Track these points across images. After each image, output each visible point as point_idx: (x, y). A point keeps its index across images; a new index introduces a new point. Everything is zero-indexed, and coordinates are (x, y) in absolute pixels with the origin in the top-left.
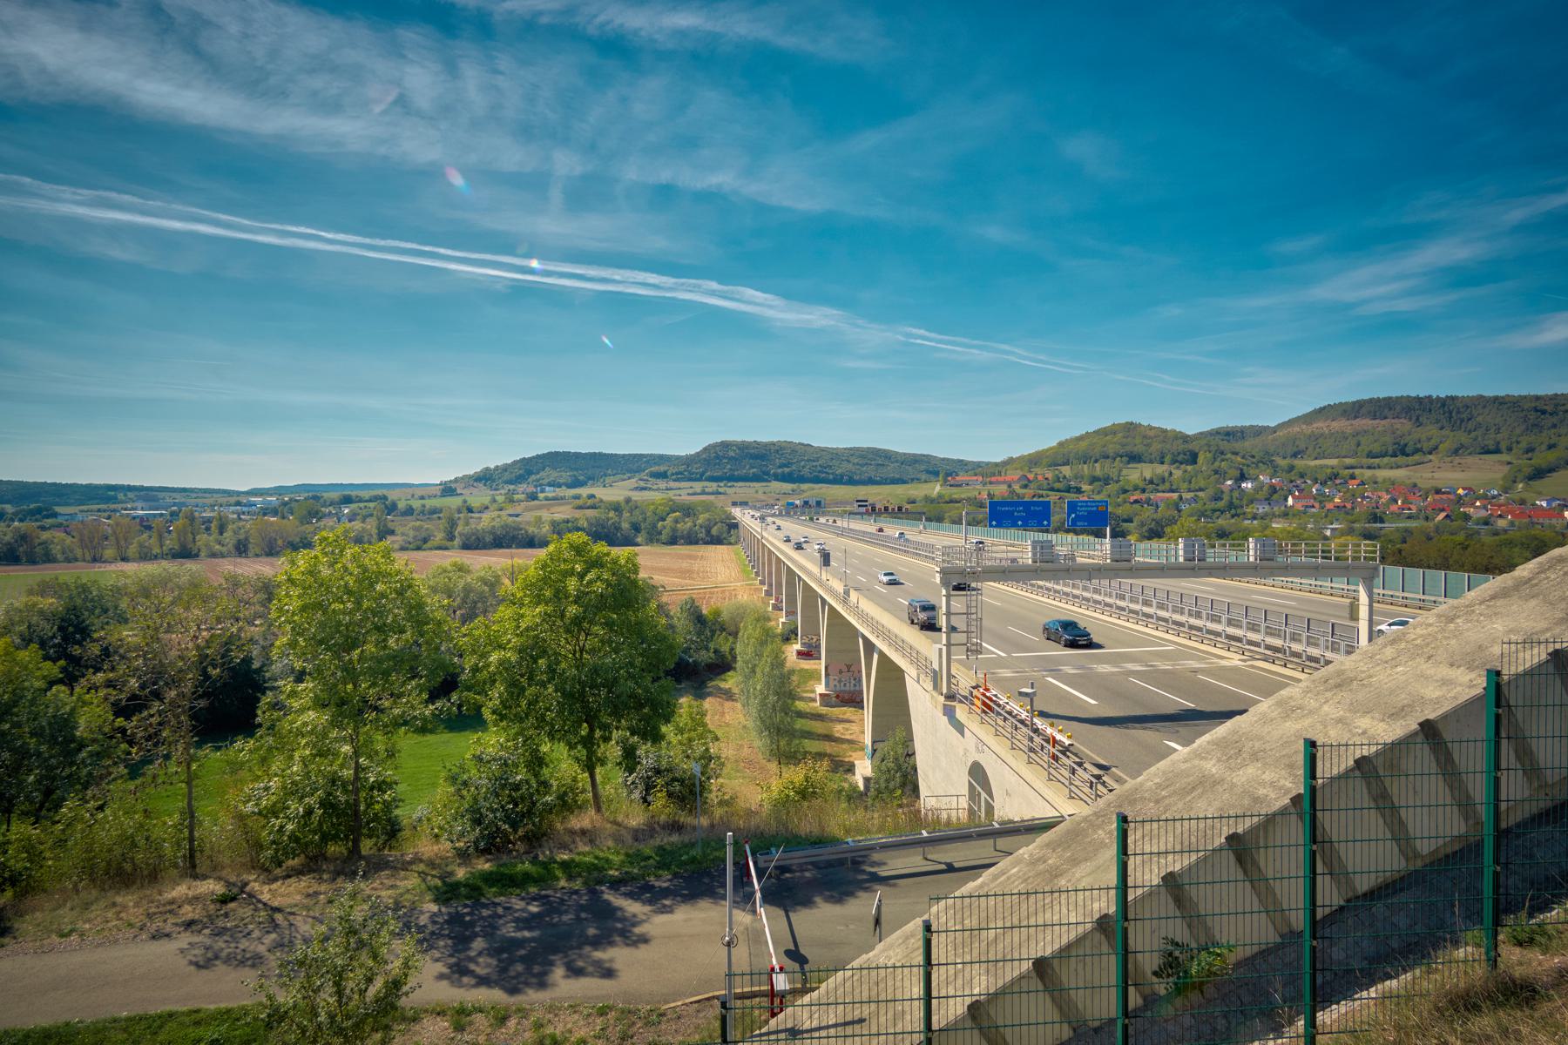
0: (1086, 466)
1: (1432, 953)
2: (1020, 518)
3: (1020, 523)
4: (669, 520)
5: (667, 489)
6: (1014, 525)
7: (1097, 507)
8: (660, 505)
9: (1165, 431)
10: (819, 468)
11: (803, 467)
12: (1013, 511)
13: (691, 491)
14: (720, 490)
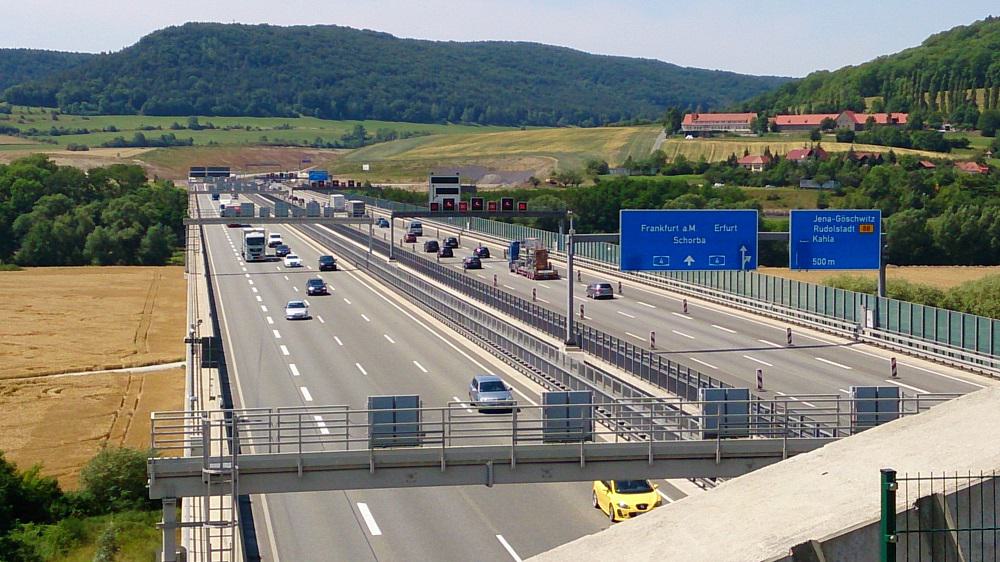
0: (980, 92)
1: (598, 199)
2: (693, 250)
3: (689, 260)
4: (40, 208)
5: (56, 133)
6: (677, 265)
7: (857, 225)
8: (20, 174)
9: (646, 60)
10: (409, 90)
11: (373, 85)
12: (673, 234)
13: (111, 137)
14: (180, 135)
